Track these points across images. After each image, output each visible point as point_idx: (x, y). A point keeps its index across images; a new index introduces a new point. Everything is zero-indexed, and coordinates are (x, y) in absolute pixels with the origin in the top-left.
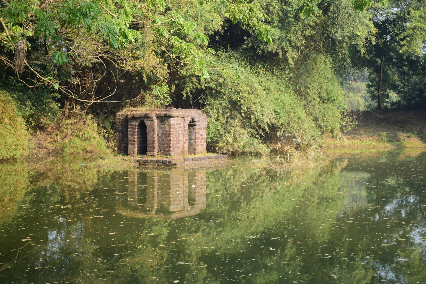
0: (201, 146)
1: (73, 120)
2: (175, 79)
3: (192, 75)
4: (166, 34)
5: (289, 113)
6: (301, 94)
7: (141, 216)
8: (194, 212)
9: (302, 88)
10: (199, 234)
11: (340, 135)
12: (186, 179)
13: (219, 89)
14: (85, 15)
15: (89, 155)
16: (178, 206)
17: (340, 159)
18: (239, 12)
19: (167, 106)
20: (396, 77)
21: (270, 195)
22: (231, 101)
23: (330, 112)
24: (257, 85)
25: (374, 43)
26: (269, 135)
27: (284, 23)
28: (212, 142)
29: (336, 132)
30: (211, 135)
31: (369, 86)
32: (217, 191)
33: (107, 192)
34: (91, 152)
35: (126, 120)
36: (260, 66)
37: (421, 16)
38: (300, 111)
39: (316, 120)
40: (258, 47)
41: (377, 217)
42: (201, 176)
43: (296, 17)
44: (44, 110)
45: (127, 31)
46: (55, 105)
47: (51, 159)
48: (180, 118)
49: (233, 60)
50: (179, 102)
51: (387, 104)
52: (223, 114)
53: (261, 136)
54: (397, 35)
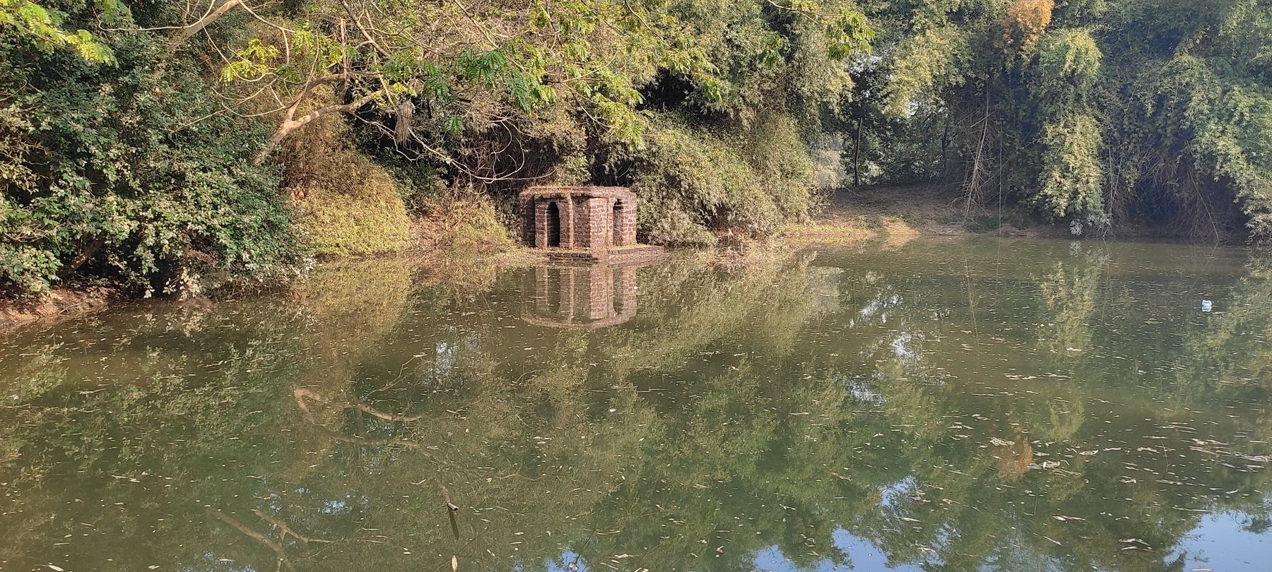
0: (630, 236)
1: (464, 202)
2: (596, 147)
3: (617, 143)
4: (588, 91)
5: (742, 190)
6: (758, 166)
7: (554, 325)
8: (620, 321)
9: (760, 159)
10: (629, 347)
11: (808, 220)
12: (611, 277)
13: (652, 160)
14: (487, 68)
15: (485, 247)
16: (601, 311)
17: (808, 250)
18: (679, 61)
19: (585, 183)
20: (877, 145)
21: (719, 297)
22: (667, 176)
23: (796, 190)
24: (700, 155)
25: (851, 100)
26: (717, 218)
27: (735, 74)
28: (644, 230)
29: (802, 215)
30: (642, 221)
31: (843, 156)
32: (651, 293)
33: (510, 293)
34: (488, 243)
35: (533, 202)
36: (705, 130)
37: (907, 67)
38: (757, 189)
39: (777, 200)
40: (703, 104)
41: (852, 322)
42: (630, 274)
43: (752, 67)
44: (428, 189)
45: (539, 88)
46: (441, 183)
47: (438, 251)
48: (602, 199)
49: (670, 122)
50: (600, 177)
51: (864, 179)
52: (657, 193)
53: (707, 221)
54: (879, 90)
